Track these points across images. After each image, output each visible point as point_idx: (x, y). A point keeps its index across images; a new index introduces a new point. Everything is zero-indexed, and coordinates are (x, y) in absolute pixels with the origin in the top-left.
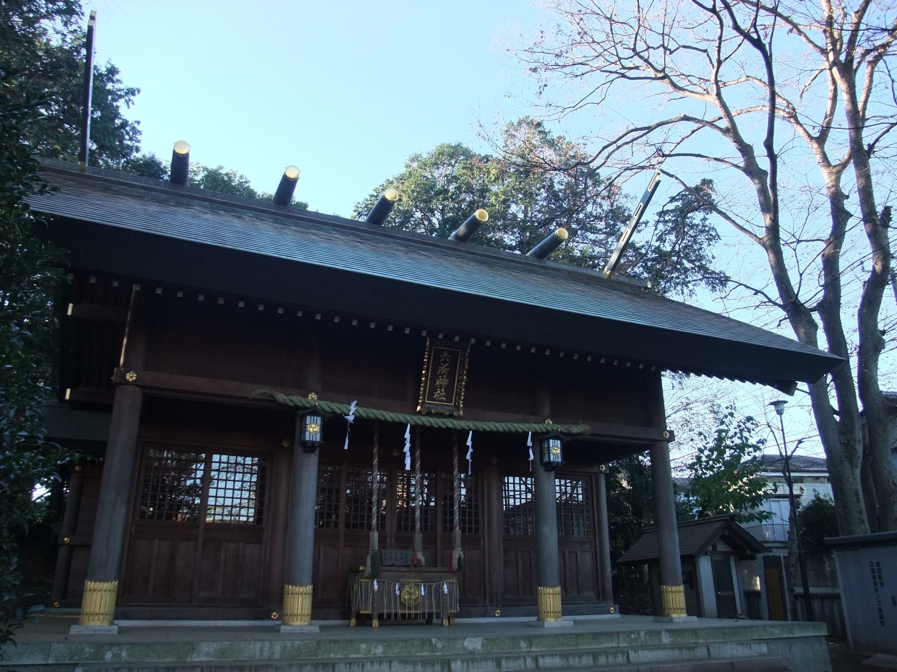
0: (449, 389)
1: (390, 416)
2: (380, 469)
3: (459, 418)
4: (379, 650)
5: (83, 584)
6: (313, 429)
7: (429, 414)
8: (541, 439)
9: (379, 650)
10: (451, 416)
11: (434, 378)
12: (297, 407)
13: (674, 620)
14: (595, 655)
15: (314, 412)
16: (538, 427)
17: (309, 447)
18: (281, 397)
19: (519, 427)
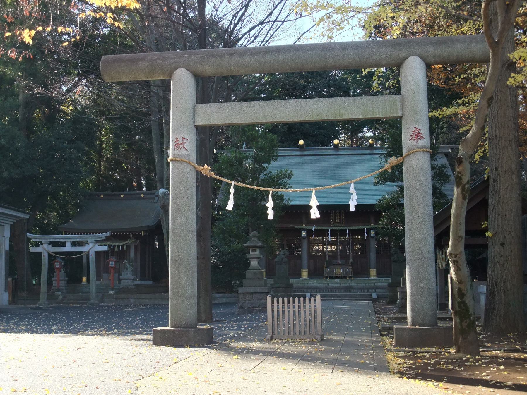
0: (340, 219)
1: (324, 228)
2: (331, 236)
3: (343, 227)
4: (315, 281)
5: (313, 219)
6: (304, 234)
7: (335, 226)
8: (369, 230)
9: (132, 301)
10: (341, 226)
11: (335, 217)
12: (300, 229)
13: (295, 286)
14: (365, 284)
15: (304, 229)
16: (368, 227)
17: (304, 238)
18: (296, 227)
19: (362, 227)
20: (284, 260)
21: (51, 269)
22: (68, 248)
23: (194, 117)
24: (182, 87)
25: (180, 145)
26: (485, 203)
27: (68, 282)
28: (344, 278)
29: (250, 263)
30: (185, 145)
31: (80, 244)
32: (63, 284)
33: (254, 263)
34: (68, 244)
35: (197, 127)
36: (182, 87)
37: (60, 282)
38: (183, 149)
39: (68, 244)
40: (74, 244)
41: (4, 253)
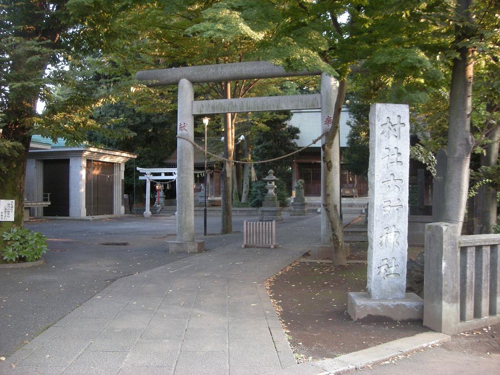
20: (301, 186)
21: (153, 190)
22: (163, 177)
23: (192, 110)
24: (186, 90)
25: (185, 127)
26: (116, 280)
27: (166, 198)
28: (352, 197)
29: (267, 191)
30: (185, 128)
31: (171, 174)
32: (162, 200)
33: (271, 192)
34: (163, 175)
35: (193, 115)
36: (186, 90)
37: (160, 199)
38: (184, 130)
39: (163, 175)
40: (166, 174)
41: (121, 181)
